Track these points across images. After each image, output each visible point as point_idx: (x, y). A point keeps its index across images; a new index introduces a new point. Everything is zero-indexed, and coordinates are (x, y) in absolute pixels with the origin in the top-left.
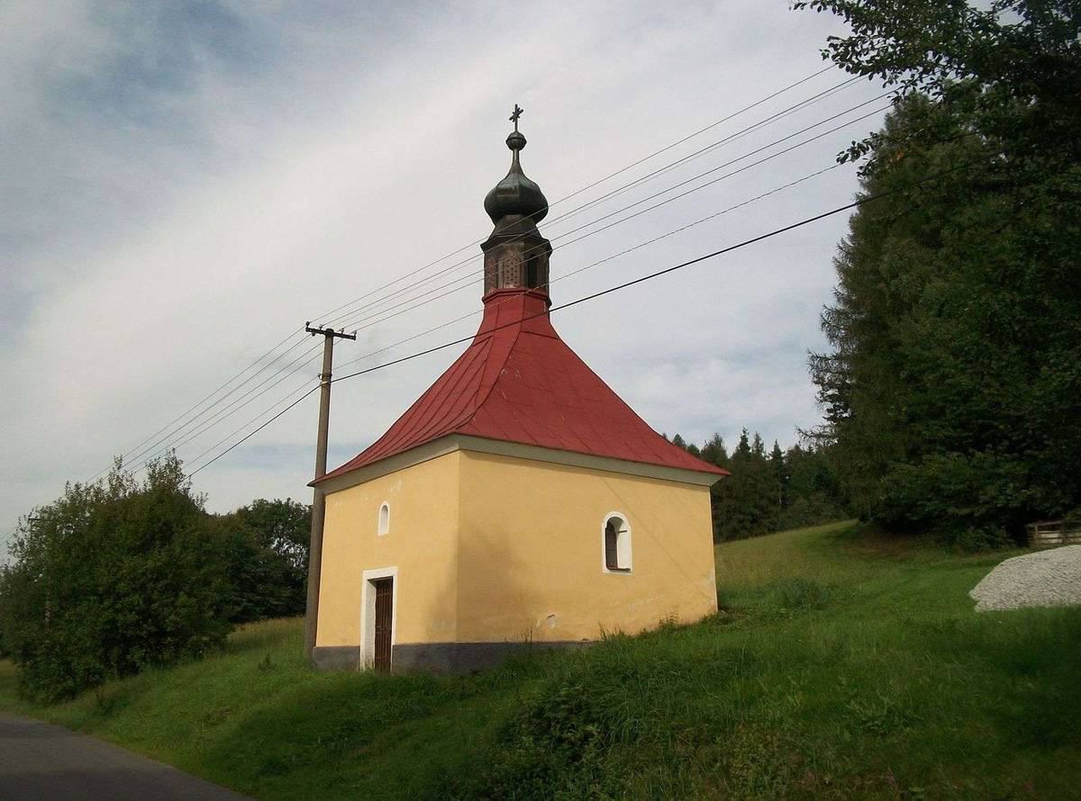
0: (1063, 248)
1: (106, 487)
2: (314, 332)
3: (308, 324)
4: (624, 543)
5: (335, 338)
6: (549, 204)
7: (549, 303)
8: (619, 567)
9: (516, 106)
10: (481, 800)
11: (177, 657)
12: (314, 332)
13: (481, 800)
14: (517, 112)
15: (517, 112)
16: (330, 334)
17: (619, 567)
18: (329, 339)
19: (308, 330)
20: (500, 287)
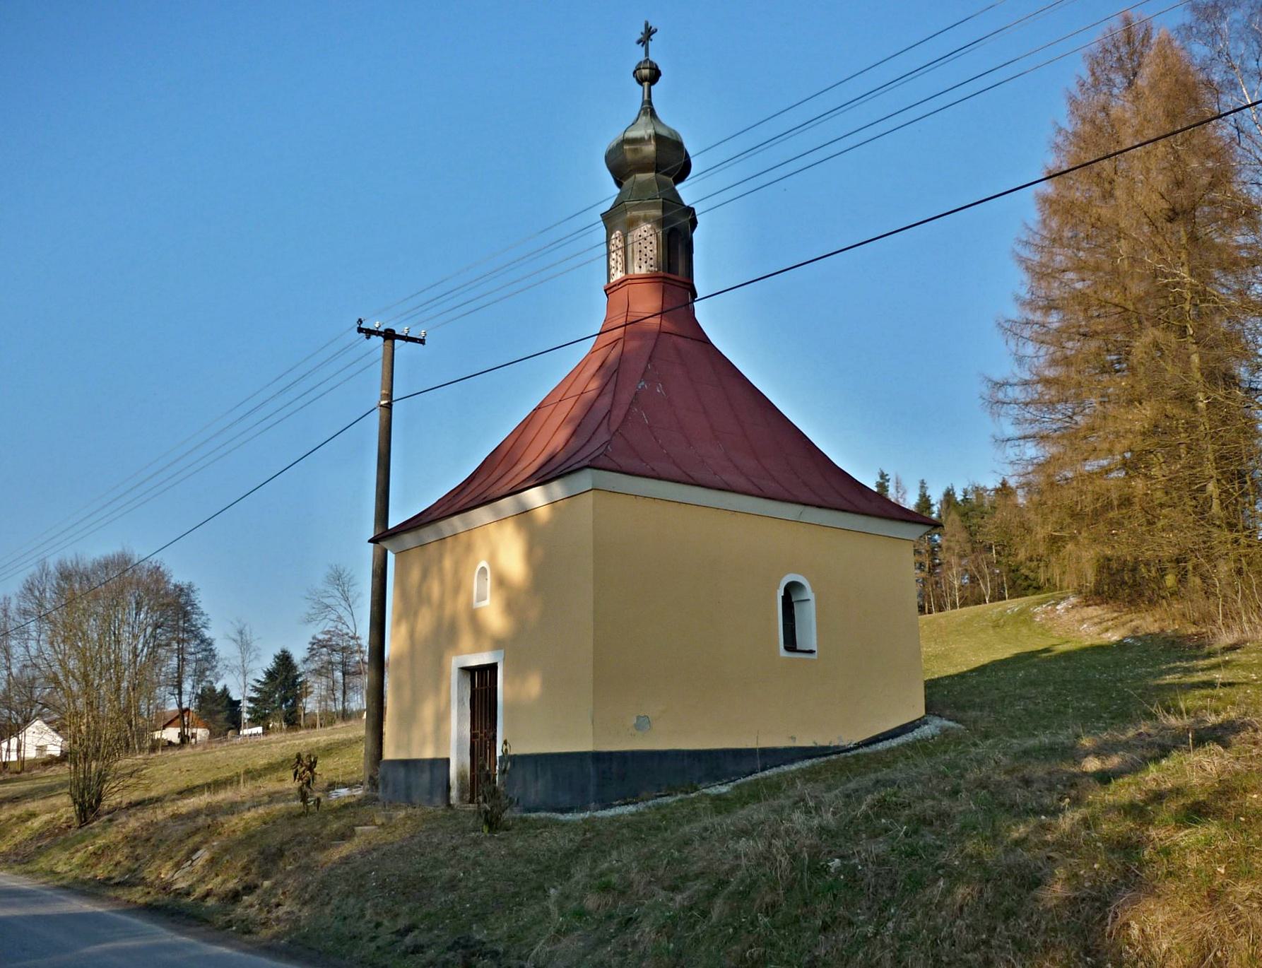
0: (680, 897)
1: (331, 572)
2: (369, 333)
3: (360, 321)
4: (807, 616)
5: (396, 341)
6: (690, 155)
7: (694, 294)
8: (798, 648)
9: (647, 24)
10: (1259, 289)
11: (1109, 560)
12: (369, 333)
13: (1259, 289)
14: (649, 33)
15: (649, 33)
16: (389, 335)
17: (798, 648)
18: (389, 342)
19: (360, 330)
20: (630, 272)
